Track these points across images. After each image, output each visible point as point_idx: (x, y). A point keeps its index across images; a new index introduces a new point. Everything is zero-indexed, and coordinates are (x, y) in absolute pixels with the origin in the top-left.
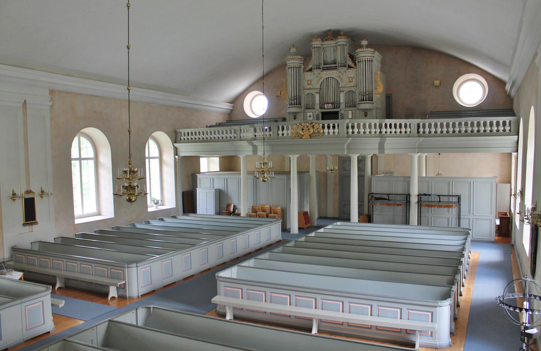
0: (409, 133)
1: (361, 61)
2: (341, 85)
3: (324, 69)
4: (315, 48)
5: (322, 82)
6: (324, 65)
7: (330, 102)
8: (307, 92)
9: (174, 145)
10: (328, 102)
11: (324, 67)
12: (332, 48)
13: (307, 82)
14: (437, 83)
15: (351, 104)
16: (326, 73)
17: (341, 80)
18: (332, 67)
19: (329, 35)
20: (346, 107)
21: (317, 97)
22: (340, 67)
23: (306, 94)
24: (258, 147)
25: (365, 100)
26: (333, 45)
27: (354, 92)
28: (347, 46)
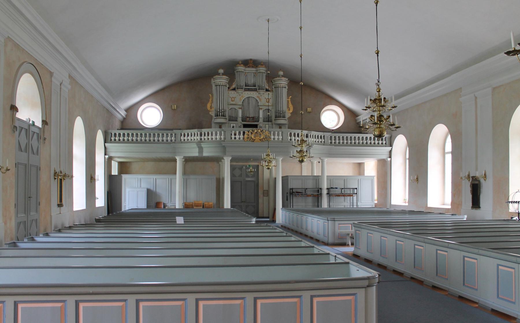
0: (323, 143)
1: (277, 87)
2: (259, 104)
3: (246, 90)
4: (260, 73)
5: (244, 100)
6: (245, 86)
7: (251, 117)
8: (231, 107)
9: (105, 145)
10: (249, 116)
11: (246, 88)
12: (253, 74)
13: (230, 98)
14: (309, 109)
15: (268, 120)
16: (248, 93)
17: (260, 99)
18: (252, 89)
19: (251, 63)
20: (263, 121)
21: (240, 112)
22: (261, 89)
23: (230, 108)
24: (204, 149)
25: (221, 116)
26: (254, 72)
27: (236, 109)
28: (265, 74)
